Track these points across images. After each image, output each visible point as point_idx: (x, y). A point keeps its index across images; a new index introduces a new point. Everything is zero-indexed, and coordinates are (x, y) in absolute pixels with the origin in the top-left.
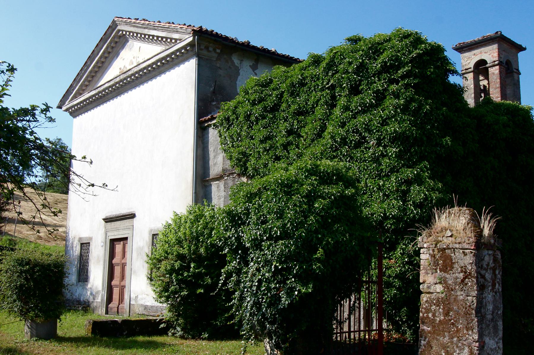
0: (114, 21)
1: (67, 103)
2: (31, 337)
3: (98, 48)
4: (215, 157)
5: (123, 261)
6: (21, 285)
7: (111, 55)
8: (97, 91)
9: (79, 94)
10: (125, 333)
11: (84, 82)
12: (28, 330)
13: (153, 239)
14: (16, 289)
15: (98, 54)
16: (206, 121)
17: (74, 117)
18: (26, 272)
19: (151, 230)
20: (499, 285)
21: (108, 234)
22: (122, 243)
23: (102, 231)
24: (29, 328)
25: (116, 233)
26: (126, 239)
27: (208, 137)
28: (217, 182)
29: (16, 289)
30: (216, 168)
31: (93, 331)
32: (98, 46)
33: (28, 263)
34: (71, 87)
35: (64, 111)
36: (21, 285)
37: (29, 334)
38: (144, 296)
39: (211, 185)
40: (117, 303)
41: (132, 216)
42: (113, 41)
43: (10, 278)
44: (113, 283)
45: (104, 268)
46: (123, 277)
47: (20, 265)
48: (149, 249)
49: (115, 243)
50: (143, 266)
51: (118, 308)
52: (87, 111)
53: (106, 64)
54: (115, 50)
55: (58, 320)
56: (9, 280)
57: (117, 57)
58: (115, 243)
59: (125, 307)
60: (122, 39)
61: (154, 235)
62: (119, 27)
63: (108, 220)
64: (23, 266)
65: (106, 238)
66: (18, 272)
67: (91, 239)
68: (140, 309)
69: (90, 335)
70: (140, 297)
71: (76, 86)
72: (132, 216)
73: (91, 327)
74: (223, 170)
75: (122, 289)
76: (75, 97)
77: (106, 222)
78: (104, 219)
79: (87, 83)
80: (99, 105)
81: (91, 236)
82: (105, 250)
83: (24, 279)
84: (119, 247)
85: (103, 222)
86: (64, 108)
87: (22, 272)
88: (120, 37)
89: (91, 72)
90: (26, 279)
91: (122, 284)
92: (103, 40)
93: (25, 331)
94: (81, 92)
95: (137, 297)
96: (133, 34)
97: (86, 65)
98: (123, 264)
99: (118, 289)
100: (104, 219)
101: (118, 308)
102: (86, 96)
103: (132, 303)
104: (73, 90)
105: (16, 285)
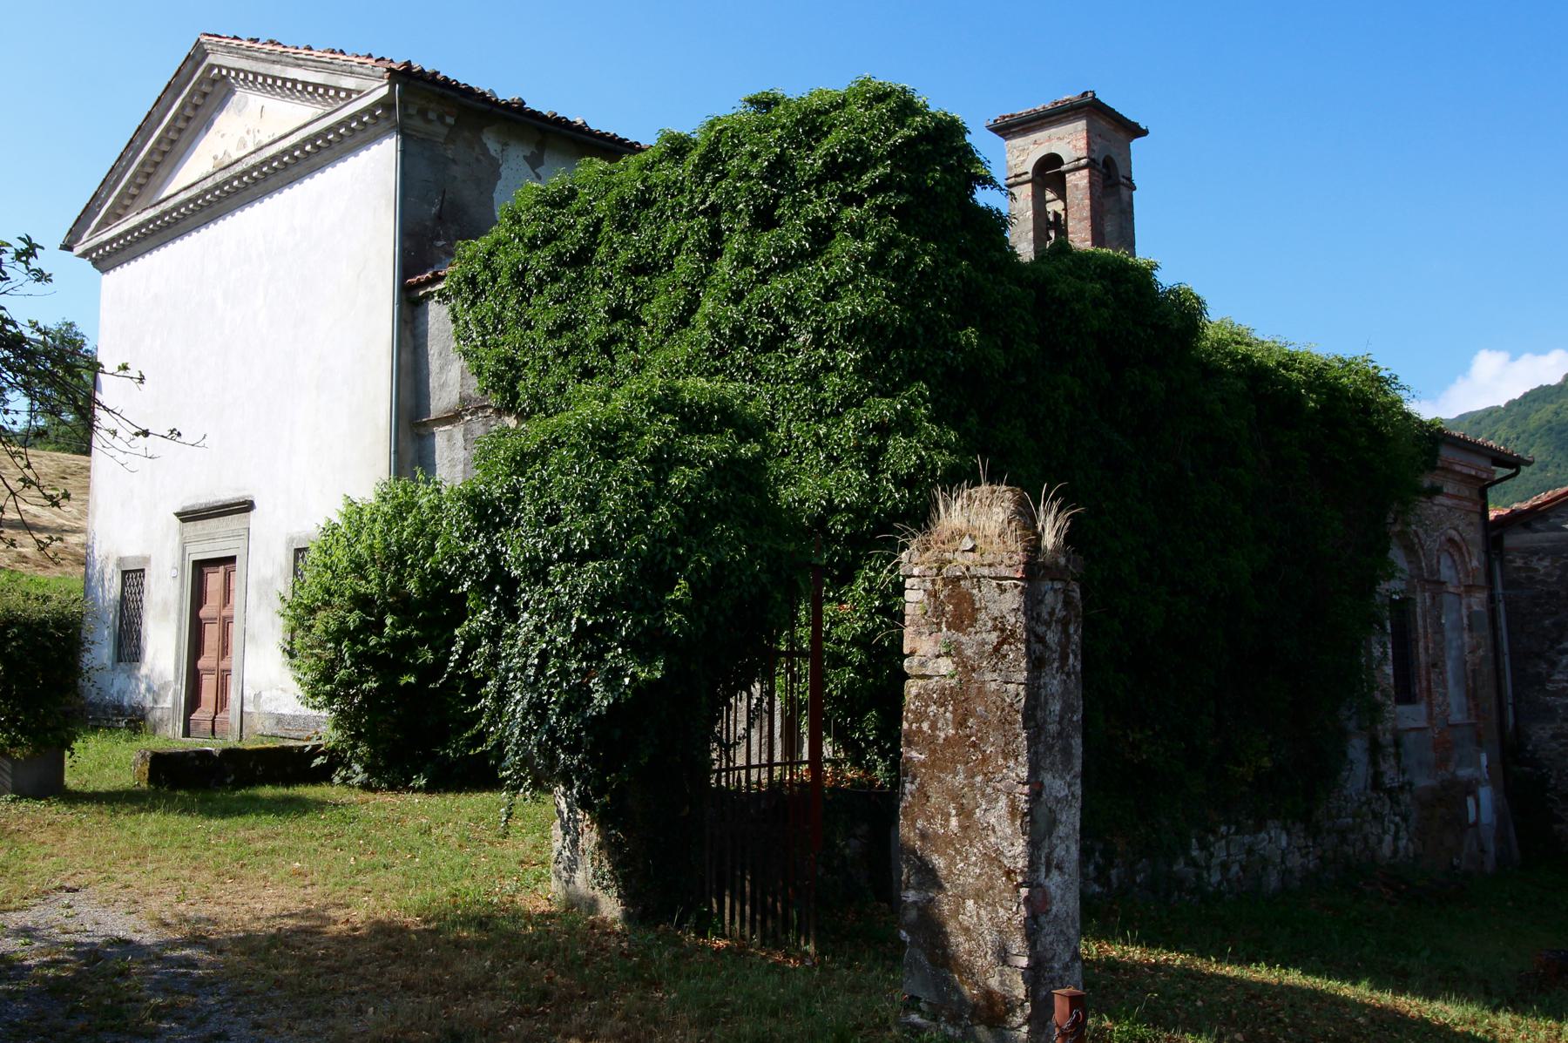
1: (85, 238)
4: (442, 368)
7: (193, 124)
11: (127, 187)
13: (296, 559)
15: (160, 123)
17: (104, 271)
19: (292, 540)
22: (222, 568)
23: (173, 543)
26: (232, 559)
32: (161, 103)
35: (84, 255)
40: (212, 710)
41: (246, 506)
42: (198, 92)
44: (201, 663)
45: (179, 629)
46: (224, 650)
49: (206, 570)
53: (181, 146)
54: (202, 112)
55: (67, 753)
57: (208, 130)
58: (206, 570)
60: (218, 86)
62: (211, 59)
63: (187, 516)
67: (147, 560)
69: (144, 785)
70: (265, 695)
71: (109, 195)
72: (246, 506)
73: (146, 767)
74: (462, 399)
75: (223, 677)
76: (105, 223)
77: (183, 521)
78: (178, 515)
81: (147, 553)
82: (182, 585)
84: (214, 580)
85: (176, 520)
86: (79, 249)
88: (214, 82)
89: (143, 164)
91: (223, 665)
92: (172, 89)
95: (258, 696)
96: (246, 77)
97: (132, 147)
100: (178, 515)
104: (101, 206)
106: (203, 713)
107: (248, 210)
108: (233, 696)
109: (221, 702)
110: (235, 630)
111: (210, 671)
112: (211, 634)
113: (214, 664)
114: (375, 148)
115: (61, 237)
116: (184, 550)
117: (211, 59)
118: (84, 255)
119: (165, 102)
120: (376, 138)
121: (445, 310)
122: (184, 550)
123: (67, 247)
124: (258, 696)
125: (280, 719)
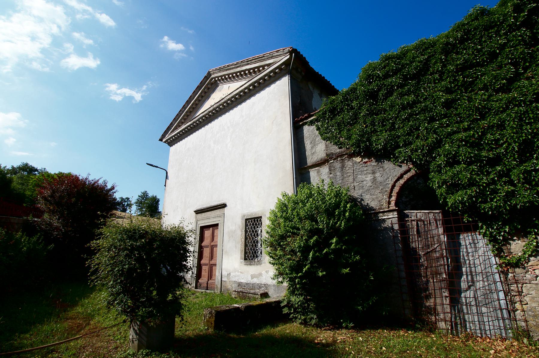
0: (209, 72)
2: (139, 349)
3: (194, 94)
4: (312, 148)
5: (212, 244)
6: (131, 270)
7: (203, 99)
8: (192, 121)
9: (179, 126)
10: (248, 323)
11: (181, 120)
12: (135, 336)
13: (246, 222)
14: (121, 275)
16: (302, 120)
17: (171, 146)
18: (138, 248)
19: (244, 216)
20: (253, 277)
21: (199, 223)
22: (211, 229)
23: (193, 220)
24: (136, 334)
25: (206, 221)
26: (217, 225)
27: (303, 133)
28: (318, 168)
29: (121, 275)
30: (314, 156)
31: (217, 326)
32: (195, 93)
33: (142, 236)
34: (171, 124)
35: (165, 142)
36: (129, 269)
37: (136, 343)
38: (237, 273)
39: (309, 172)
40: (206, 279)
41: (224, 206)
42: (208, 86)
43: (113, 258)
44: (203, 262)
46: (212, 257)
47: (130, 238)
48: (242, 232)
50: (236, 247)
51: (207, 283)
52: (181, 140)
53: (199, 105)
54: (207, 94)
55: (177, 320)
56: (112, 262)
59: (216, 283)
60: (213, 85)
61: (246, 220)
62: (213, 76)
63: (198, 212)
64: (136, 240)
65: (196, 226)
66: (126, 249)
68: (233, 285)
69: (211, 330)
72: (224, 206)
73: (213, 320)
74: (327, 155)
75: (211, 267)
77: (197, 214)
78: (195, 211)
79: (183, 121)
80: (192, 133)
83: (135, 260)
84: (208, 233)
85: (194, 214)
86: (164, 140)
87: (133, 249)
88: (212, 84)
89: (187, 112)
90: (139, 260)
91: (212, 262)
92: (199, 88)
93: (131, 337)
94: (180, 124)
95: (229, 274)
96: (225, 77)
97: (184, 107)
98: (212, 246)
99: (207, 267)
100: (195, 211)
101: (207, 283)
102: (183, 127)
103: (223, 279)
105: (122, 270)
106: (203, 280)
107: (223, 116)
108: (217, 274)
109: (211, 275)
110: (218, 250)
111: (206, 265)
112: (206, 252)
113: (208, 262)
114: (278, 83)
115: (160, 137)
116: (197, 223)
117: (213, 76)
118: (165, 142)
119: (195, 93)
120: (284, 75)
121: (314, 128)
122: (197, 223)
123: (161, 140)
124: (229, 274)
125: (240, 284)
